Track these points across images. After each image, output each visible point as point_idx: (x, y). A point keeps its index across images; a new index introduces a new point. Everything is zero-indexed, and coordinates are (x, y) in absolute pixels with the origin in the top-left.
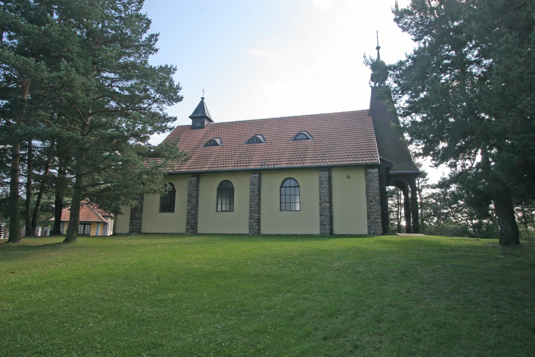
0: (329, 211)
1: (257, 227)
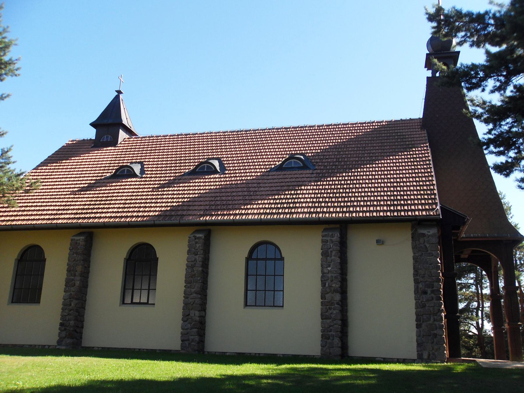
0: (340, 311)
1: (197, 338)
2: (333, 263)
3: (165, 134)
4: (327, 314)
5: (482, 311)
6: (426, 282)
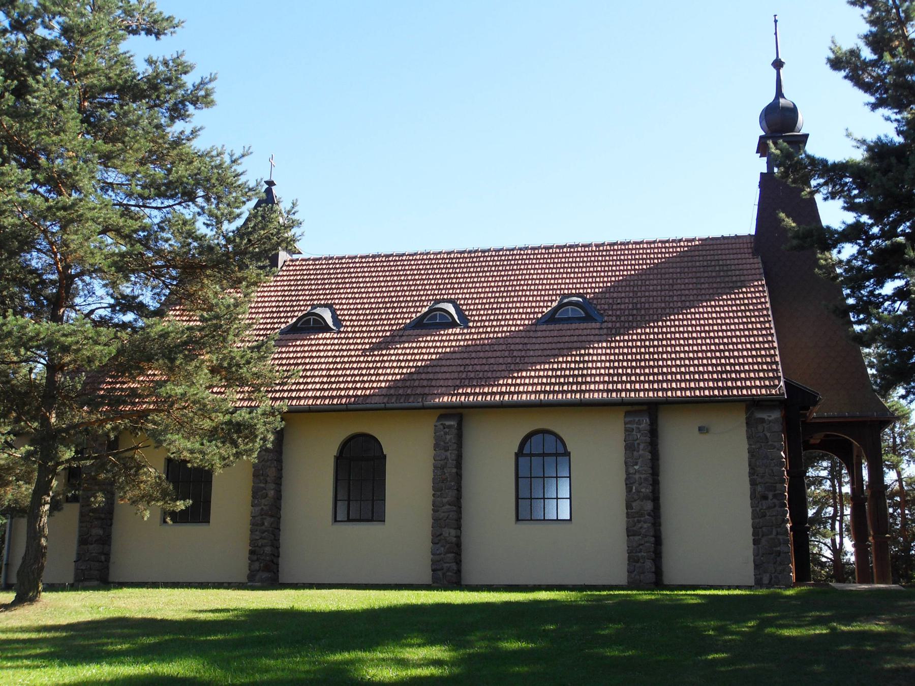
0: (652, 524)
1: (454, 566)
2: (641, 460)
3: (353, 254)
4: (634, 528)
5: (841, 522)
6: (767, 483)
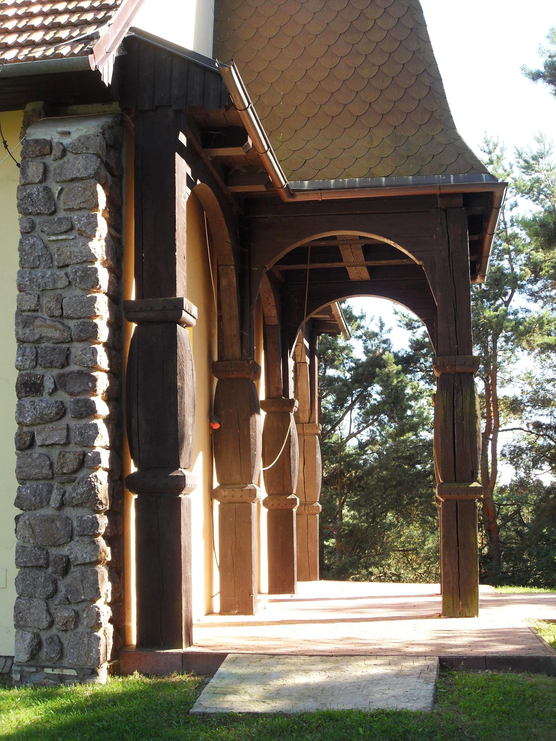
6: (38, 341)
